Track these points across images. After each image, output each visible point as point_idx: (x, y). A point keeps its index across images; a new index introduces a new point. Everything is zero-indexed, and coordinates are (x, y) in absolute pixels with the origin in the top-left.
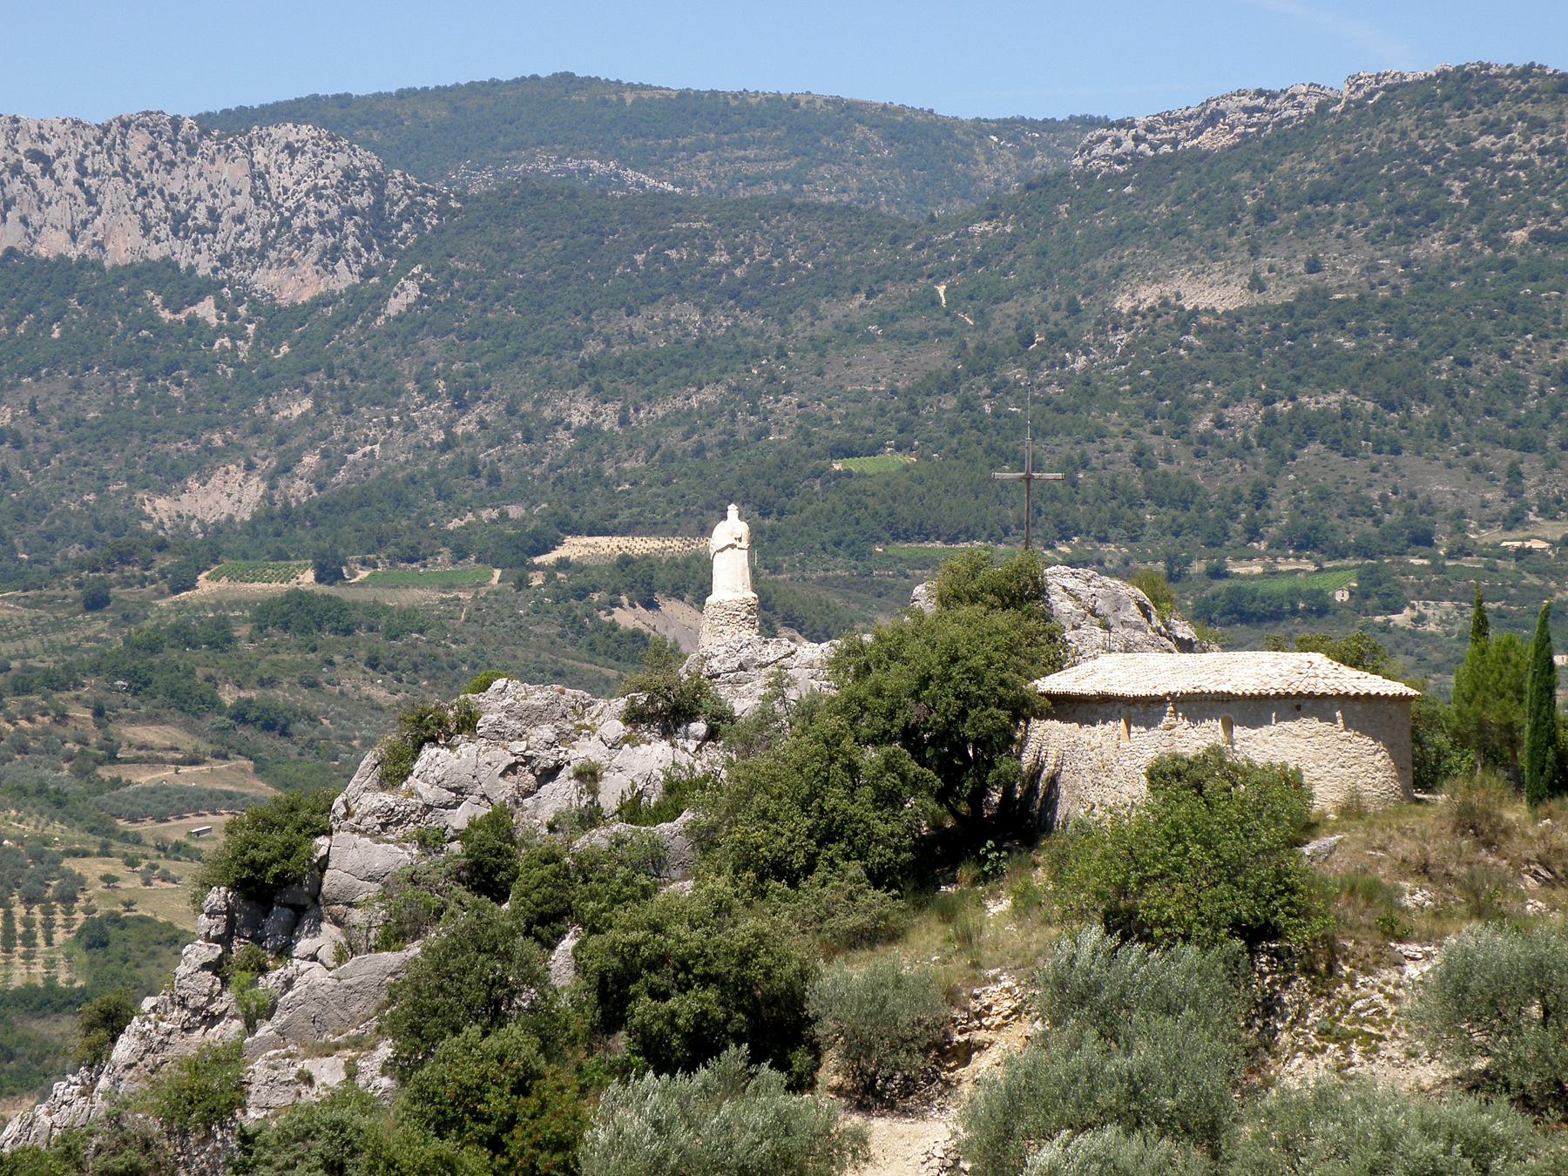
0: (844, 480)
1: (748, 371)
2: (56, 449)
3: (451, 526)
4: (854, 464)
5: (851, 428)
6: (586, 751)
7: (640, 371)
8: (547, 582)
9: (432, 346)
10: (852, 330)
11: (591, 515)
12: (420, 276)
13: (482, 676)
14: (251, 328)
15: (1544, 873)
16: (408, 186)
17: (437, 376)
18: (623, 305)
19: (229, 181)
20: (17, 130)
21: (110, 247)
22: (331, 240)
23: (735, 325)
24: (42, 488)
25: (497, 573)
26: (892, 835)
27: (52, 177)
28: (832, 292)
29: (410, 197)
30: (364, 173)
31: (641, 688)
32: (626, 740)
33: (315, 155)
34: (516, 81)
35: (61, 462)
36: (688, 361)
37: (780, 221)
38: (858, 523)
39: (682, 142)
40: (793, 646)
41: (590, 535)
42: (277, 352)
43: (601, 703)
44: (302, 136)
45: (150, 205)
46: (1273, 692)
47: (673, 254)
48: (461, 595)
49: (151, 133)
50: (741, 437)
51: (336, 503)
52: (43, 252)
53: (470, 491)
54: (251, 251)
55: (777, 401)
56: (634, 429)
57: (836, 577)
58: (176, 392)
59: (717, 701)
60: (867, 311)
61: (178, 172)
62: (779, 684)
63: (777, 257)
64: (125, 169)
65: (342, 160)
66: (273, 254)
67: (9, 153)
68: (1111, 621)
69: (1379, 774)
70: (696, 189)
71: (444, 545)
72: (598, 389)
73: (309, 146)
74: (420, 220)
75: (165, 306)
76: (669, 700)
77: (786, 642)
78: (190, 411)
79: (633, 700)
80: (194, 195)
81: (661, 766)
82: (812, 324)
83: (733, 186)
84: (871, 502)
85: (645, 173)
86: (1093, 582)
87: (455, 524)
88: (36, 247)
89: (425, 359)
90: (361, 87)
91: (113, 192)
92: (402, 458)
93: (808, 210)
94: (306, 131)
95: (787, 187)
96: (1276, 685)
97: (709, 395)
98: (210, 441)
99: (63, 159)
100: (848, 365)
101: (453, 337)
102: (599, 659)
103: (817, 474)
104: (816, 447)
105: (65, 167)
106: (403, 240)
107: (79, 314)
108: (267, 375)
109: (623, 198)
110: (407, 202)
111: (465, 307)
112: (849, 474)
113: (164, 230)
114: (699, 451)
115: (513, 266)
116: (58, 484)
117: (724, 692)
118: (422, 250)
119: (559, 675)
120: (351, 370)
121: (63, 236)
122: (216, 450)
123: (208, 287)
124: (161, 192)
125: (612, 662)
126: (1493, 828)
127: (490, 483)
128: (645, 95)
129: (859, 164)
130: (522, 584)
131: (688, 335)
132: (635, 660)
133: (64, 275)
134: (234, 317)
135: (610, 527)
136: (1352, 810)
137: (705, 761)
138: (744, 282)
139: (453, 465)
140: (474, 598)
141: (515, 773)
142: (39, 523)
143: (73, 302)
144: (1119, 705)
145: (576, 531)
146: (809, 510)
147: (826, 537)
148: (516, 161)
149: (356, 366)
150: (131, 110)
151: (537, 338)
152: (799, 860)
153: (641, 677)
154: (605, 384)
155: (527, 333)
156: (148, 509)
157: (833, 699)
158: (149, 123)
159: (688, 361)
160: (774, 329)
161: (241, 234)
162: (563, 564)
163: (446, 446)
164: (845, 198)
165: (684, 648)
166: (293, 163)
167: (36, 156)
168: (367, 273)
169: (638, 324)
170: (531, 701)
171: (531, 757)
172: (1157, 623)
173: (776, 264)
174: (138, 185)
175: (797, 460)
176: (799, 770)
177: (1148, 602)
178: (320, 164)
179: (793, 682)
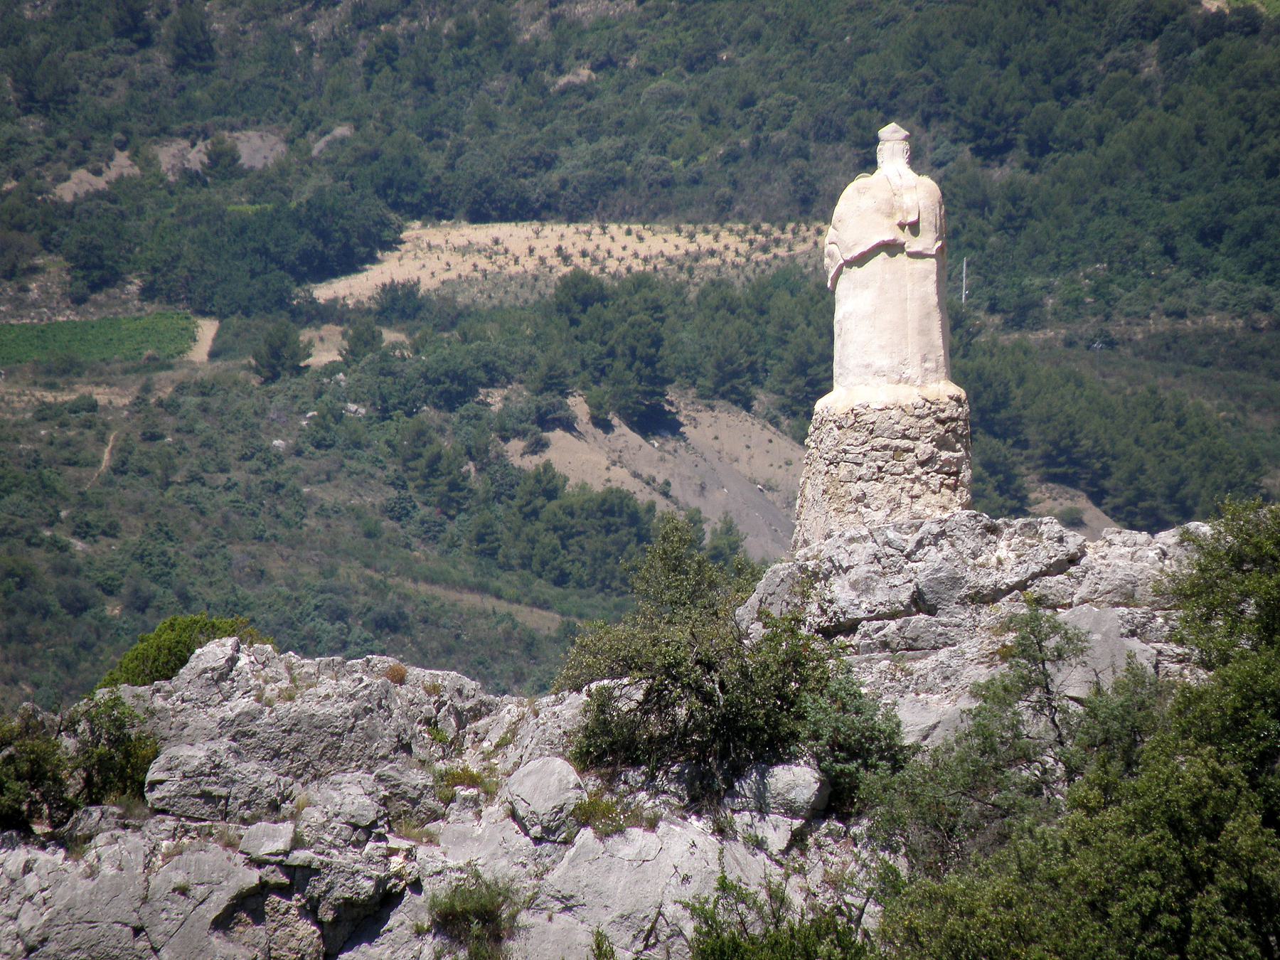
3: (66, 192)
6: (472, 847)
11: (479, 162)
13: (161, 633)
25: (207, 329)
31: (627, 666)
32: (585, 816)
40: (1074, 539)
41: (478, 216)
43: (510, 709)
48: (101, 396)
53: (121, 87)
57: (1206, 336)
59: (849, 701)
62: (1033, 651)
71: (48, 245)
76: (708, 698)
77: (1051, 527)
79: (604, 701)
81: (688, 893)
87: (75, 185)
102: (507, 581)
117: (870, 674)
119: (389, 627)
125: (542, 588)
127: (181, 64)
130: (280, 362)
132: (605, 582)
137: (815, 877)
140: (140, 402)
141: (258, 917)
145: (436, 209)
147: (1174, 215)
153: (626, 632)
157: (1192, 698)
162: (400, 303)
165: (753, 547)
170: (306, 705)
171: (307, 871)
176: (1097, 908)
179: (1074, 646)
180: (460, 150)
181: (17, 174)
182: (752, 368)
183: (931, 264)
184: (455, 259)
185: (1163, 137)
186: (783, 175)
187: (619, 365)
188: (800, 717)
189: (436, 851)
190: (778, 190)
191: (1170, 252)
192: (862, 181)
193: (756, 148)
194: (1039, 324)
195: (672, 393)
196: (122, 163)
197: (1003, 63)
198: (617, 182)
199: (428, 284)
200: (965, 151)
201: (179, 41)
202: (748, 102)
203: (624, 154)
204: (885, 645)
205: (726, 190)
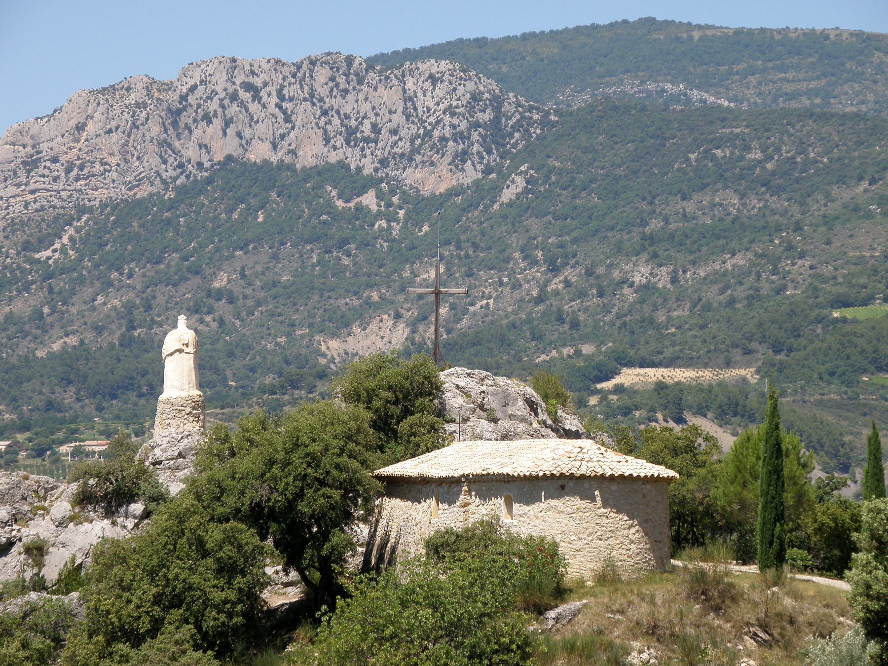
0: (840, 325)
1: (772, 241)
2: (259, 304)
4: (849, 313)
5: (851, 285)
6: (39, 529)
7: (688, 242)
8: (600, 402)
9: (534, 225)
10: (856, 209)
11: (644, 352)
12: (526, 172)
14: (402, 213)
15: (762, 634)
16: (519, 105)
17: (537, 247)
18: (679, 192)
19: (387, 104)
20: (235, 68)
21: (300, 153)
22: (461, 147)
23: (765, 207)
24: (248, 333)
26: (226, 601)
27: (259, 102)
28: (842, 180)
29: (520, 113)
30: (486, 95)
32: (72, 519)
33: (450, 83)
34: (611, 25)
35: (262, 313)
36: (726, 234)
37: (803, 126)
38: (848, 358)
39: (736, 68)
41: (641, 366)
42: (420, 231)
44: (442, 69)
45: (329, 122)
46: (541, 474)
47: (718, 153)
49: (331, 69)
50: (764, 292)
51: (456, 343)
52: (253, 158)
53: (556, 333)
54: (402, 155)
55: (793, 264)
56: (681, 286)
57: (830, 400)
58: (346, 261)
59: (156, 485)
60: (870, 195)
61: (350, 97)
63: (800, 154)
64: (312, 96)
65: (471, 86)
66: (418, 158)
67: (229, 85)
68: (499, 414)
69: (633, 546)
70: (745, 103)
72: (655, 255)
73: (446, 77)
74: (527, 131)
75: (340, 197)
78: (356, 275)
80: (362, 114)
82: (826, 205)
83: (775, 101)
84: (859, 341)
85: (707, 92)
86: (487, 382)
88: (248, 154)
89: (528, 234)
90: (495, 32)
91: (303, 113)
92: (509, 309)
93: (825, 117)
94: (445, 65)
95: (818, 101)
96: (547, 468)
97: (740, 260)
98: (369, 297)
99: (268, 89)
100: (851, 236)
101: (550, 217)
103: (819, 320)
104: (820, 299)
105: (269, 95)
106: (514, 146)
107: (277, 203)
108: (412, 248)
109: (681, 111)
110: (518, 117)
111: (559, 195)
112: (844, 320)
113: (340, 141)
114: (732, 302)
115: (596, 164)
116: (259, 330)
118: (529, 153)
120: (473, 243)
121: (267, 145)
122: (374, 303)
123: (372, 182)
124: (338, 112)
126: (722, 594)
127: (571, 328)
128: (709, 33)
129: (875, 82)
131: (728, 214)
133: (267, 175)
134: (389, 205)
135: (657, 361)
136: (608, 577)
138: (773, 173)
139: (544, 314)
142: (245, 359)
143: (274, 195)
144: (434, 486)
145: (630, 364)
146: (810, 348)
147: (822, 369)
148: (608, 85)
149: (477, 241)
150: (316, 51)
151: (613, 218)
152: (144, 625)
154: (661, 253)
155: (605, 214)
156: (323, 348)
158: (330, 61)
159: (726, 234)
160: (795, 209)
161: (396, 143)
162: (619, 389)
163: (540, 300)
164: (864, 108)
166: (434, 89)
167: (248, 87)
168: (487, 171)
169: (690, 207)
172: (543, 416)
173: (799, 160)
174: (321, 107)
175: (804, 309)
177: (537, 397)
178: (455, 90)
180: (639, 349)
181: (528, 356)
182: (707, 406)
183: (192, 356)
184: (635, 377)
185: (820, 348)
186: (722, 356)
187: (671, 405)
188: (139, 489)
189: (27, 530)
190: (721, 360)
191: (821, 378)
192: (174, 331)
193: (715, 350)
194: (785, 396)
195: (685, 413)
196: (554, 353)
197: (781, 329)
198: (678, 358)
199: (627, 384)
200: (770, 352)
201: (571, 322)
202: (714, 338)
203: (681, 351)
204: (169, 468)
205: (707, 360)
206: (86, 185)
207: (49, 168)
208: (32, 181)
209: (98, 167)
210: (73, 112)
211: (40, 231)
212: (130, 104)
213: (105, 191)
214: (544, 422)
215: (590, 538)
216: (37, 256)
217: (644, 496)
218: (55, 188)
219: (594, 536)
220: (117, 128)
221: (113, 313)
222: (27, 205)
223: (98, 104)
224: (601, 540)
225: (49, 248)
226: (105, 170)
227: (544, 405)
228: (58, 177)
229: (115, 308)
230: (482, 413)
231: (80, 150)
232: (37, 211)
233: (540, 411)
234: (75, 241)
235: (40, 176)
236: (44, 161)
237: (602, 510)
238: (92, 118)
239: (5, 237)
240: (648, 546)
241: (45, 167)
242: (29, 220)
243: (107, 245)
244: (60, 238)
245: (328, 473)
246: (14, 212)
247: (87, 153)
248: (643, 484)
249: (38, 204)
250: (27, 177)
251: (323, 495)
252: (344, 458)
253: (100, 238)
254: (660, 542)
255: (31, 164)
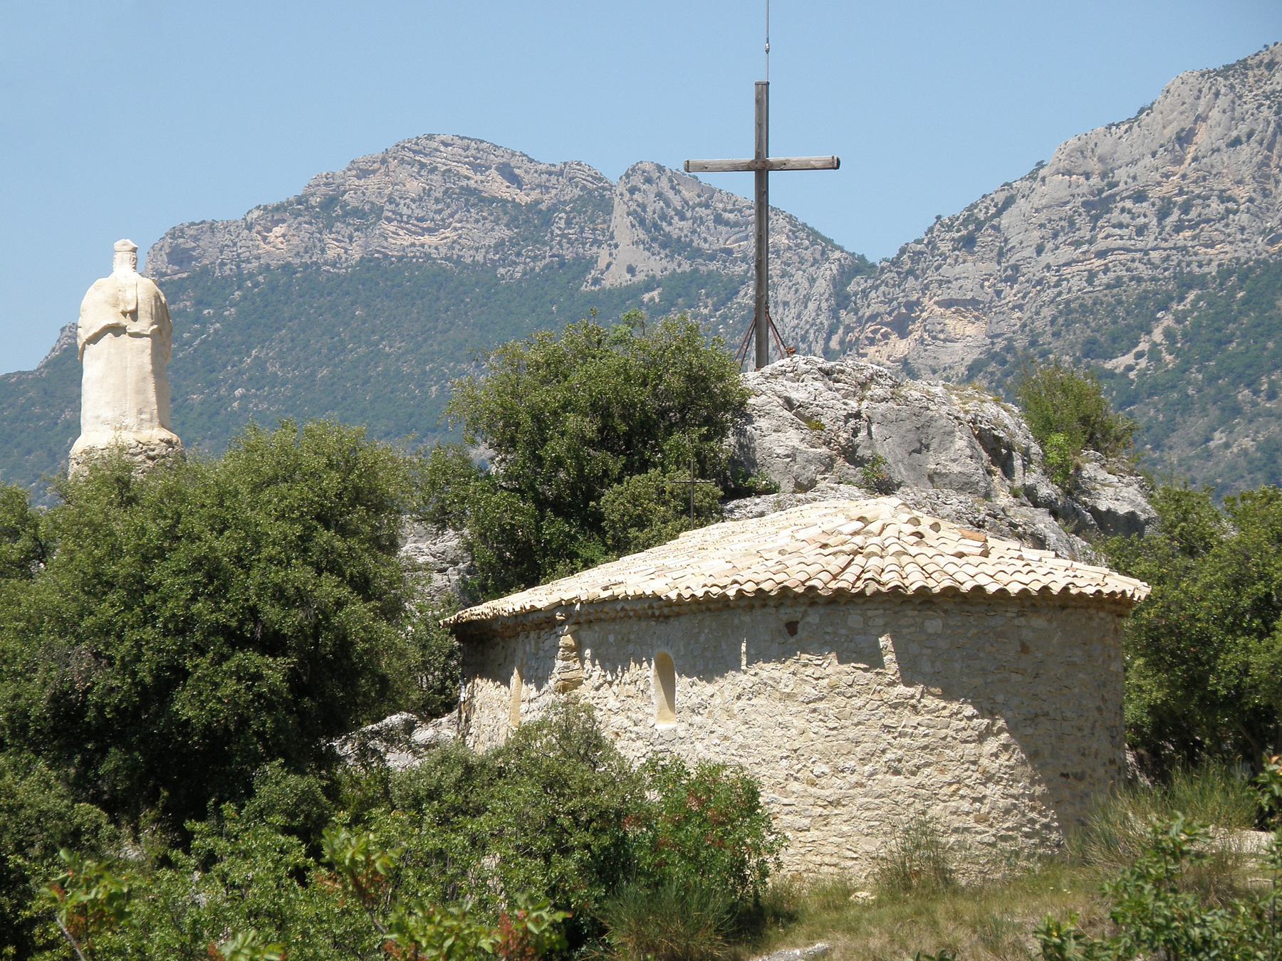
46: (731, 592)
68: (899, 473)
69: (993, 791)
136: (918, 877)
183: (147, 342)
206: (1194, 238)
207: (1129, 212)
208: (1100, 236)
209: (1216, 207)
210: (1172, 111)
211: (1114, 322)
212: (1273, 92)
213: (1228, 248)
214: (1030, 494)
215: (868, 769)
216: (1109, 365)
217: (1024, 649)
218: (1140, 245)
219: (879, 763)
220: (1250, 135)
221: (1242, 462)
222: (1092, 276)
223: (1217, 94)
224: (897, 772)
225: (1128, 351)
226: (1228, 211)
227: (1035, 448)
228: (1145, 226)
229: (1245, 452)
230: (852, 470)
231: (1184, 177)
232: (1108, 286)
233: (1018, 463)
234: (1175, 336)
235: (1114, 226)
236: (1122, 199)
237: (901, 689)
238: (1204, 120)
239: (1054, 335)
240: (1039, 790)
241: (1123, 210)
242: (1095, 304)
243: (1231, 342)
244: (1149, 333)
245: (253, 612)
246: (1070, 290)
247: (1195, 182)
248: (1021, 614)
249: (1111, 275)
250: (1093, 229)
251: (237, 673)
252: (301, 574)
253: (1219, 330)
254: (1080, 777)
255: (1098, 206)
